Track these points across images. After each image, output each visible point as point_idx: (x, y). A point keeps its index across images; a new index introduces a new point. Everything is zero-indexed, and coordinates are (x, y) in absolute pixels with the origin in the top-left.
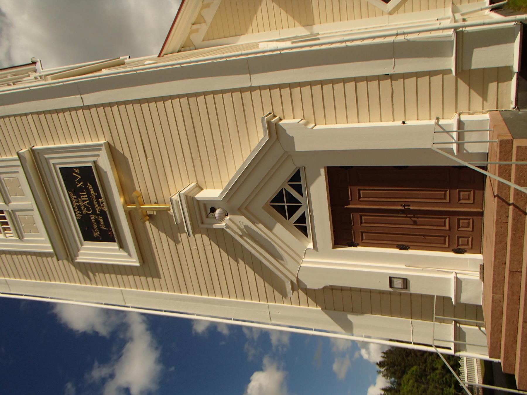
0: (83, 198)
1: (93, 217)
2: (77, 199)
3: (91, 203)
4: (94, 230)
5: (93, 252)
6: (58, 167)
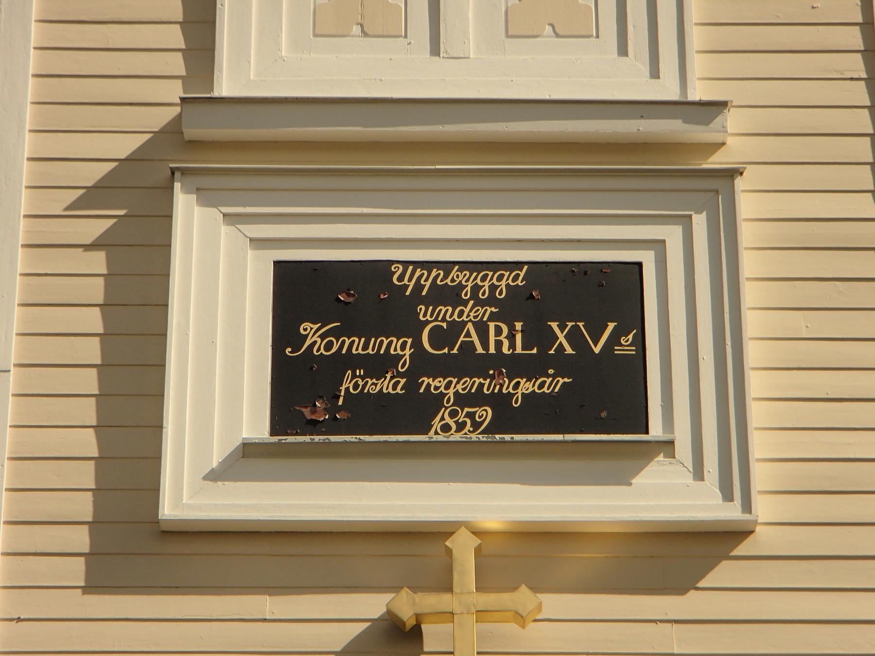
0: (498, 331)
1: (400, 347)
2: (492, 300)
3: (467, 363)
4: (336, 333)
5: (220, 288)
6: (647, 259)
